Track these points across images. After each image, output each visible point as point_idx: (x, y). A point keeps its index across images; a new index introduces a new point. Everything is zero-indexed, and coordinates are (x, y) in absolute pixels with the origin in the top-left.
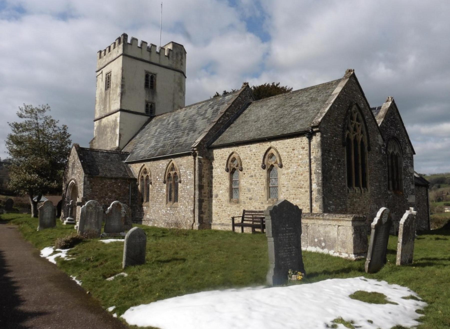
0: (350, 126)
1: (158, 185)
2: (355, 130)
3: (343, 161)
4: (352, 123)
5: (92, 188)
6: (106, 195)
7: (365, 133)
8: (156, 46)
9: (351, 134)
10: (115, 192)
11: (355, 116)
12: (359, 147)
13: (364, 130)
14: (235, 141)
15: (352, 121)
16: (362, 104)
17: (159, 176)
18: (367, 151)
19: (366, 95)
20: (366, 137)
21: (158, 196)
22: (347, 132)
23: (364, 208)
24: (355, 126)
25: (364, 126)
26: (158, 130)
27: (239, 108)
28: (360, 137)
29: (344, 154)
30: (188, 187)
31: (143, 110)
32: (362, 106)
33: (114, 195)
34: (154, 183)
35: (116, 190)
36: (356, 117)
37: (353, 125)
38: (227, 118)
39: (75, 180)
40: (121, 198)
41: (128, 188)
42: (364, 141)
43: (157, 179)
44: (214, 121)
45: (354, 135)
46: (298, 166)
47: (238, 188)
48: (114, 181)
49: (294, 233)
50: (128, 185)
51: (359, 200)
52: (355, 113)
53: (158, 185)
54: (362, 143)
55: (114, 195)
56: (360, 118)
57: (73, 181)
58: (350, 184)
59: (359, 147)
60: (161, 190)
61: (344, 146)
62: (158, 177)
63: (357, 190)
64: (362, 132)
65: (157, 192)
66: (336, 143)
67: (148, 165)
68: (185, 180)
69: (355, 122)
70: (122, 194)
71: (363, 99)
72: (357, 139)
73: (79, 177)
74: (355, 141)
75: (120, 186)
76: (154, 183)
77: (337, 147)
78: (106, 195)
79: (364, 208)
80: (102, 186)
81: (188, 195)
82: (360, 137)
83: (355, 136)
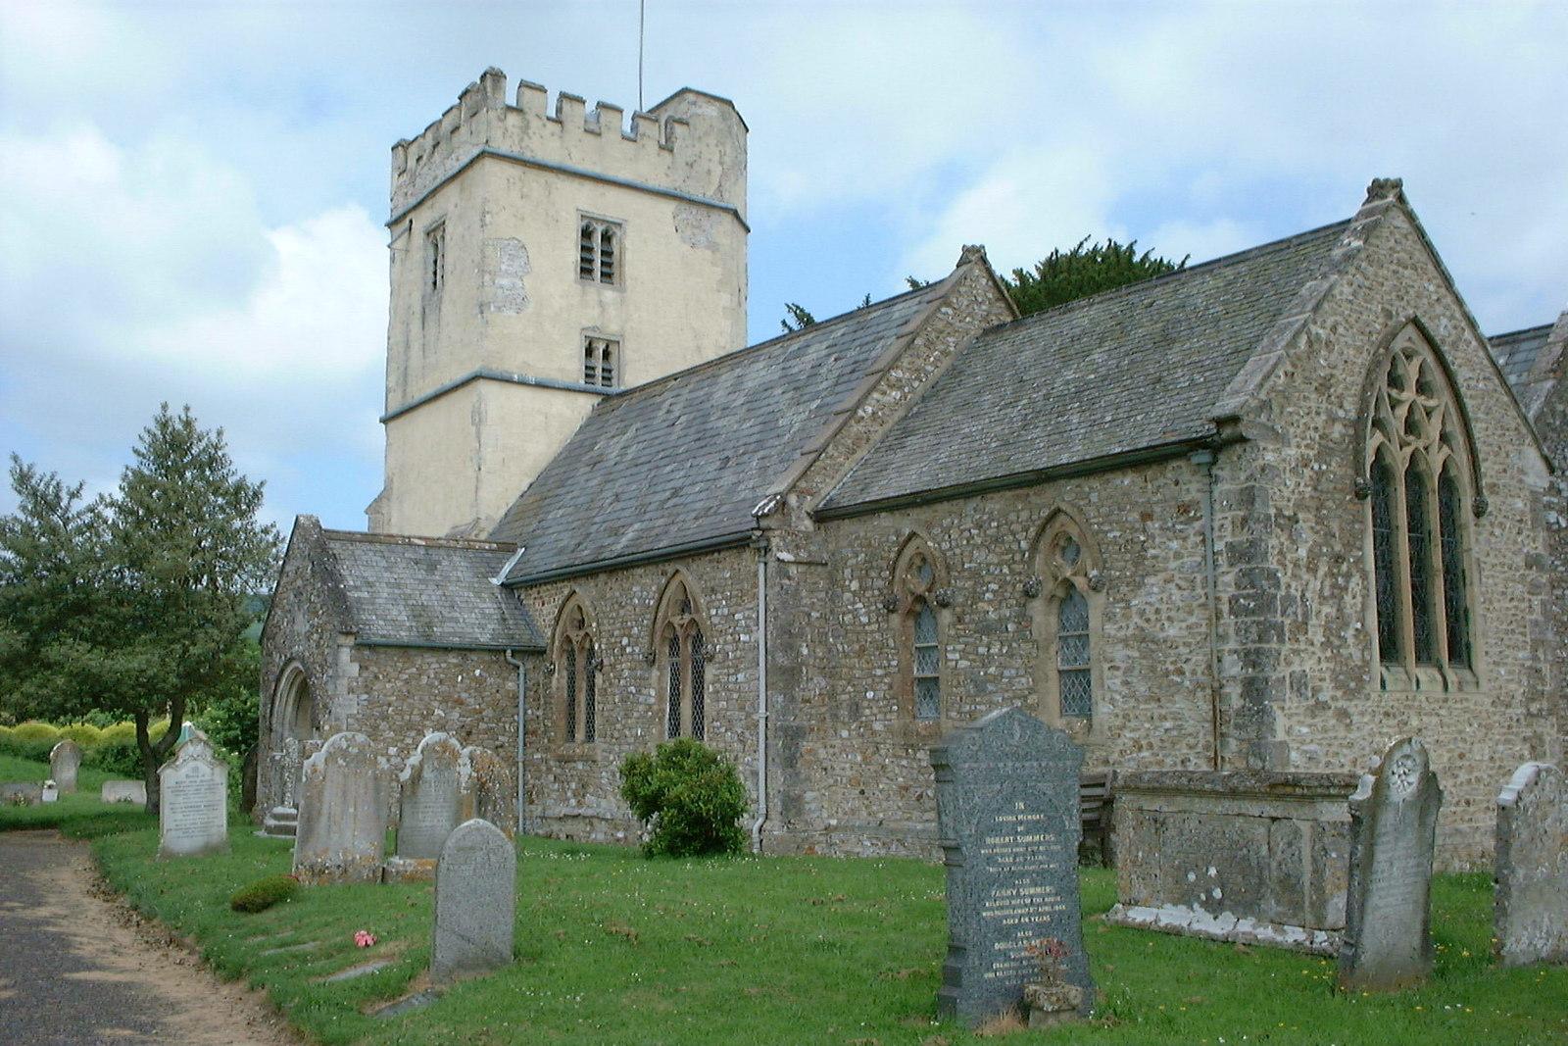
0: (1385, 411)
1: (626, 673)
2: (1411, 427)
3: (1360, 560)
4: (1394, 404)
5: (368, 690)
6: (424, 717)
7: (1459, 440)
8: (542, 90)
9: (1394, 447)
10: (460, 702)
11: (1411, 372)
12: (1433, 504)
13: (1455, 427)
14: (920, 488)
15: (1394, 393)
16: (1444, 321)
17: (629, 636)
18: (1471, 516)
19: (1459, 286)
20: (1462, 458)
21: (627, 716)
22: (1374, 440)
23: (1461, 756)
24: (1411, 410)
25: (1452, 410)
26: (632, 452)
27: (945, 353)
28: (1436, 460)
29: (1363, 531)
30: (741, 676)
31: (572, 368)
32: (1441, 329)
33: (455, 715)
34: (613, 666)
35: (464, 695)
36: (1414, 376)
37: (1402, 411)
38: (896, 394)
39: (303, 661)
40: (482, 726)
41: (510, 685)
42: (1453, 472)
43: (623, 648)
44: (839, 407)
45: (1408, 450)
46: (1167, 581)
47: (936, 679)
48: (455, 661)
49: (1051, 837)
50: (513, 675)
51: (1435, 720)
52: (1409, 357)
53: (626, 673)
54: (1447, 483)
55: (455, 715)
56: (1436, 377)
57: (296, 664)
58: (1389, 650)
59: (1433, 504)
60: (639, 692)
61: (1360, 495)
62: (625, 641)
63: (1423, 678)
64: (1444, 438)
65: (622, 700)
66: (1324, 485)
67: (586, 593)
68: (729, 647)
69: (1409, 395)
70: (488, 713)
71: (1449, 299)
72: (1422, 466)
73: (318, 646)
74: (1415, 477)
75: (480, 681)
76: (613, 666)
77: (1330, 504)
78: (424, 717)
79: (1461, 756)
80: (407, 682)
81: (742, 709)
82: (1436, 460)
83: (1413, 455)
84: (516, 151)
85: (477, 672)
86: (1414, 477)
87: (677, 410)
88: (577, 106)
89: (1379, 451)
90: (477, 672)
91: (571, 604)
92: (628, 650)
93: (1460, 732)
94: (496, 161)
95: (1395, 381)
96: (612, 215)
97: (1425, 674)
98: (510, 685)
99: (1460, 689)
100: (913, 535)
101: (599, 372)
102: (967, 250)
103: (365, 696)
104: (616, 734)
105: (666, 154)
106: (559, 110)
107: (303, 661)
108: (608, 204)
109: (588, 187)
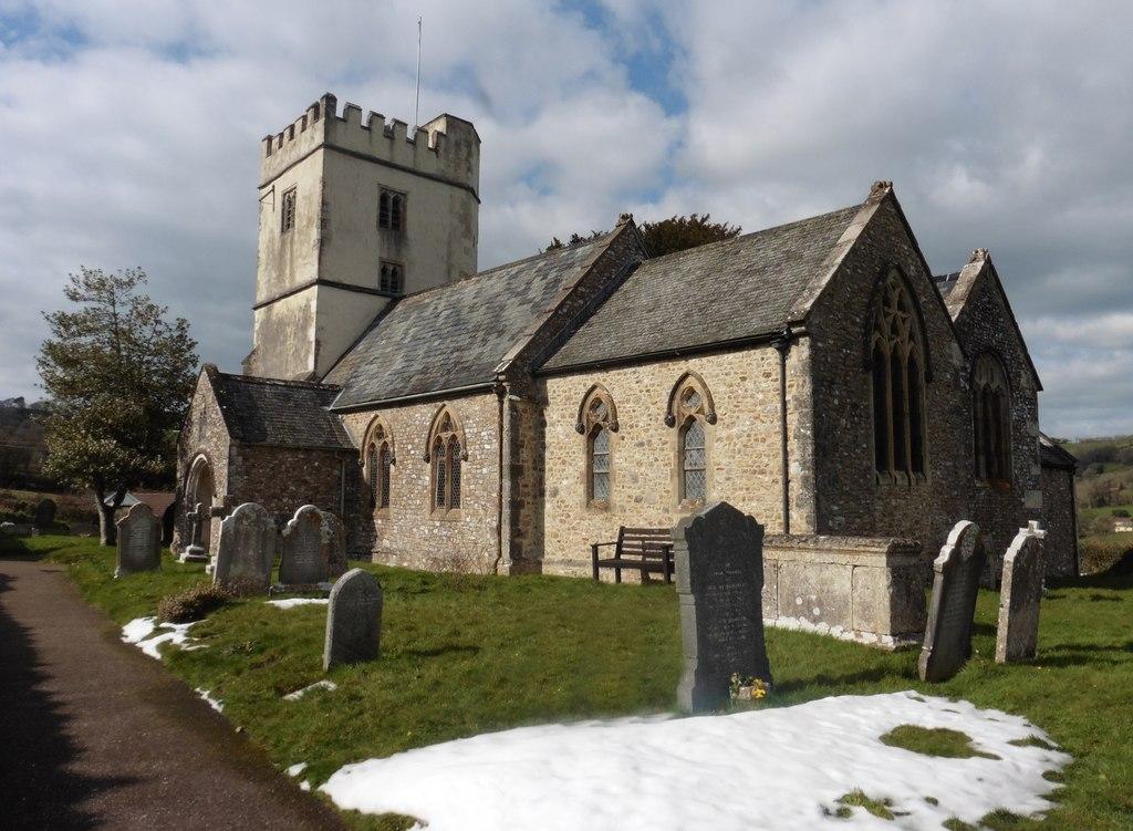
0: (882, 320)
2: (895, 330)
5: (247, 473)
7: (919, 337)
9: (885, 341)
11: (894, 296)
12: (905, 373)
16: (912, 268)
17: (413, 444)
24: (894, 320)
28: (906, 349)
30: (485, 471)
35: (308, 478)
37: (890, 319)
39: (207, 455)
41: (336, 472)
44: (548, 308)
45: (893, 343)
50: (338, 466)
56: (908, 301)
57: (202, 456)
58: (882, 464)
59: (905, 373)
60: (419, 478)
61: (867, 369)
63: (898, 477)
64: (911, 337)
69: (894, 310)
70: (322, 488)
75: (318, 469)
78: (282, 490)
79: (917, 522)
80: (272, 469)
82: (906, 349)
84: (410, 165)
85: (316, 464)
86: (896, 359)
87: (440, 308)
88: (380, 120)
89: (911, 353)
90: (316, 464)
91: (375, 424)
92: (412, 452)
93: (916, 508)
94: (380, 166)
95: (887, 302)
96: (398, 187)
97: (897, 474)
98: (336, 472)
99: (917, 484)
100: (594, 387)
101: (389, 284)
102: (624, 217)
103: (246, 477)
104: (403, 503)
105: (388, 141)
106: (370, 122)
107: (207, 455)
108: (398, 181)
109: (385, 170)
